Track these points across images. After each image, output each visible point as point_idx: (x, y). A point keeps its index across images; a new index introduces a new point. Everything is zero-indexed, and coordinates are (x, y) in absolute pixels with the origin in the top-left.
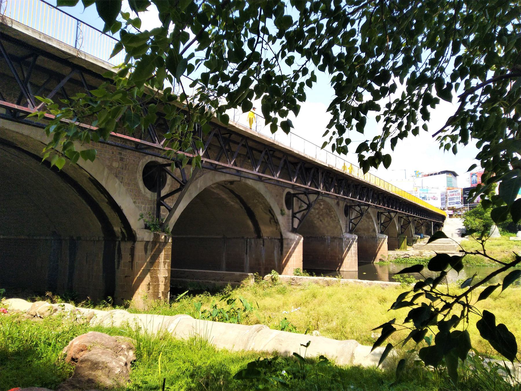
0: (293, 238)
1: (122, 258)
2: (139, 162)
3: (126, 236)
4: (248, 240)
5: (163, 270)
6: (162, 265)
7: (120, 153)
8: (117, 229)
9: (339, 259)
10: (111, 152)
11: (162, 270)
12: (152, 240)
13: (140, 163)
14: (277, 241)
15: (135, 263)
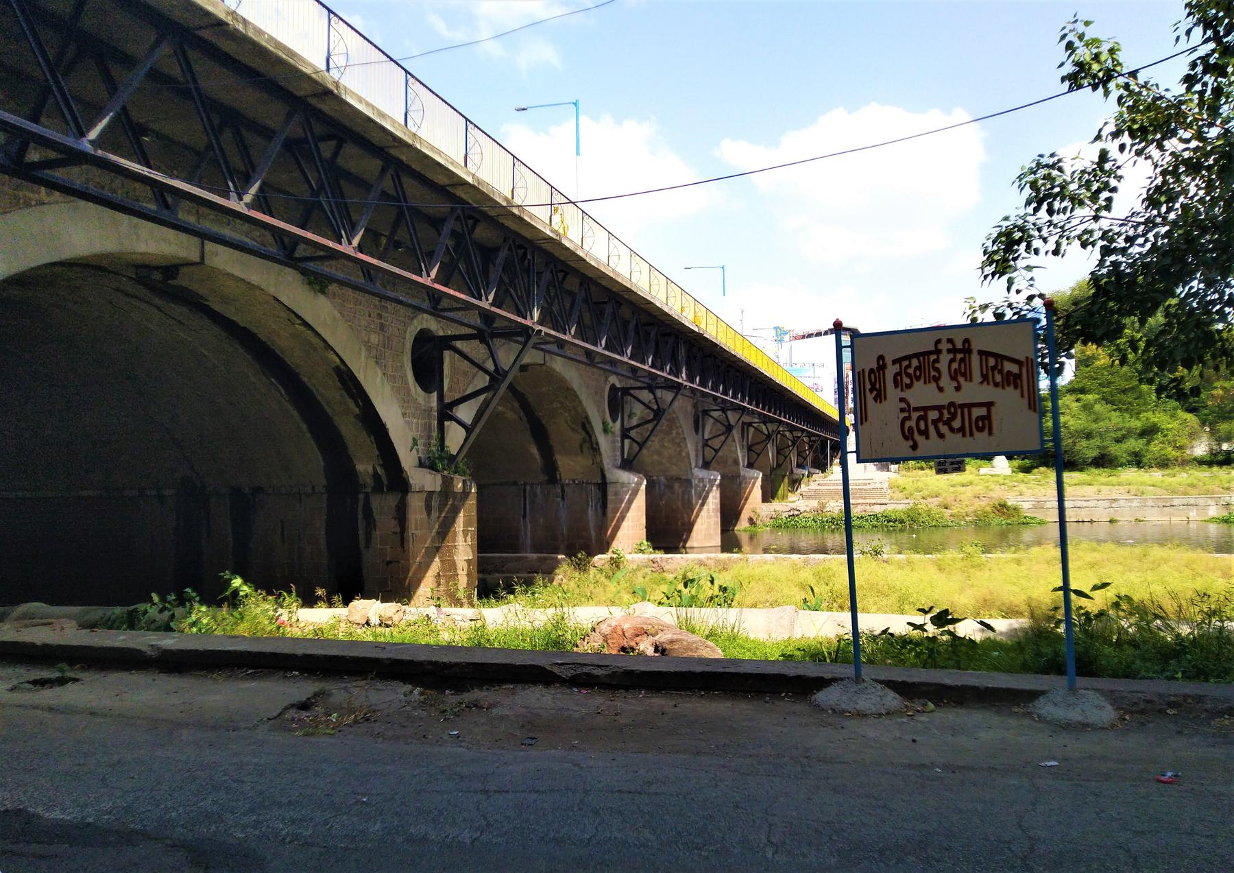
0: (626, 481)
1: (375, 526)
2: (405, 332)
3: (385, 482)
4: (528, 488)
5: (463, 545)
6: (460, 537)
7: (379, 314)
8: (365, 467)
9: (683, 524)
10: (367, 315)
11: (461, 548)
12: (438, 489)
13: (408, 336)
15: (410, 535)
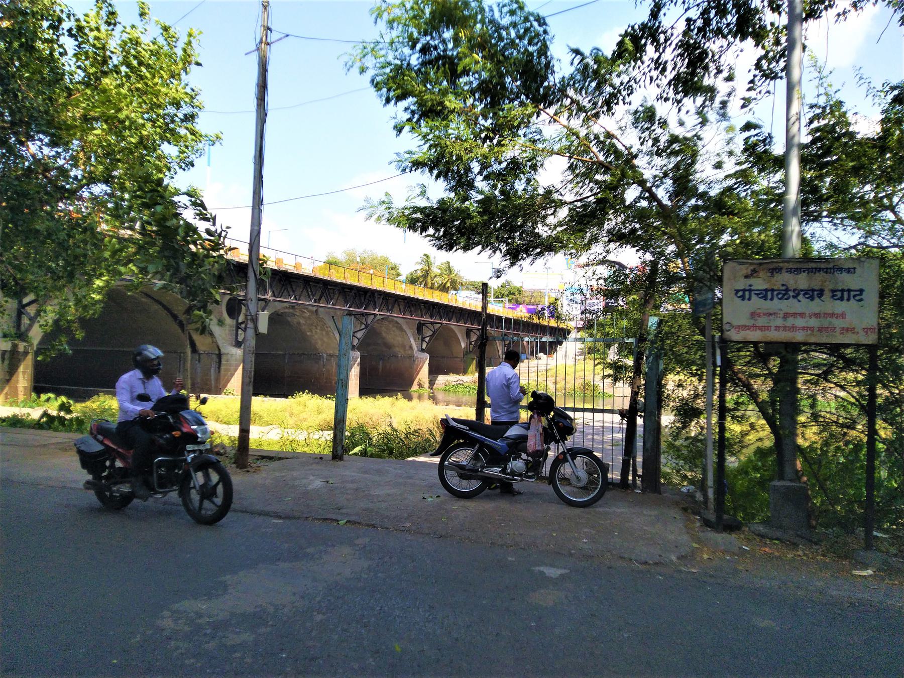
6: (21, 377)
14: (214, 356)
